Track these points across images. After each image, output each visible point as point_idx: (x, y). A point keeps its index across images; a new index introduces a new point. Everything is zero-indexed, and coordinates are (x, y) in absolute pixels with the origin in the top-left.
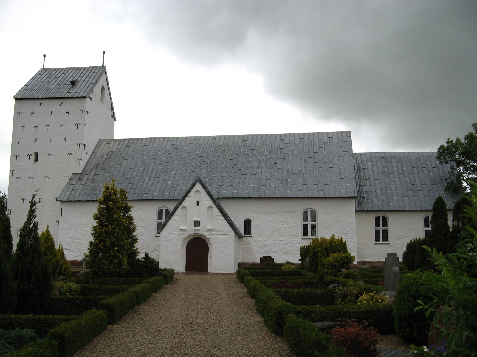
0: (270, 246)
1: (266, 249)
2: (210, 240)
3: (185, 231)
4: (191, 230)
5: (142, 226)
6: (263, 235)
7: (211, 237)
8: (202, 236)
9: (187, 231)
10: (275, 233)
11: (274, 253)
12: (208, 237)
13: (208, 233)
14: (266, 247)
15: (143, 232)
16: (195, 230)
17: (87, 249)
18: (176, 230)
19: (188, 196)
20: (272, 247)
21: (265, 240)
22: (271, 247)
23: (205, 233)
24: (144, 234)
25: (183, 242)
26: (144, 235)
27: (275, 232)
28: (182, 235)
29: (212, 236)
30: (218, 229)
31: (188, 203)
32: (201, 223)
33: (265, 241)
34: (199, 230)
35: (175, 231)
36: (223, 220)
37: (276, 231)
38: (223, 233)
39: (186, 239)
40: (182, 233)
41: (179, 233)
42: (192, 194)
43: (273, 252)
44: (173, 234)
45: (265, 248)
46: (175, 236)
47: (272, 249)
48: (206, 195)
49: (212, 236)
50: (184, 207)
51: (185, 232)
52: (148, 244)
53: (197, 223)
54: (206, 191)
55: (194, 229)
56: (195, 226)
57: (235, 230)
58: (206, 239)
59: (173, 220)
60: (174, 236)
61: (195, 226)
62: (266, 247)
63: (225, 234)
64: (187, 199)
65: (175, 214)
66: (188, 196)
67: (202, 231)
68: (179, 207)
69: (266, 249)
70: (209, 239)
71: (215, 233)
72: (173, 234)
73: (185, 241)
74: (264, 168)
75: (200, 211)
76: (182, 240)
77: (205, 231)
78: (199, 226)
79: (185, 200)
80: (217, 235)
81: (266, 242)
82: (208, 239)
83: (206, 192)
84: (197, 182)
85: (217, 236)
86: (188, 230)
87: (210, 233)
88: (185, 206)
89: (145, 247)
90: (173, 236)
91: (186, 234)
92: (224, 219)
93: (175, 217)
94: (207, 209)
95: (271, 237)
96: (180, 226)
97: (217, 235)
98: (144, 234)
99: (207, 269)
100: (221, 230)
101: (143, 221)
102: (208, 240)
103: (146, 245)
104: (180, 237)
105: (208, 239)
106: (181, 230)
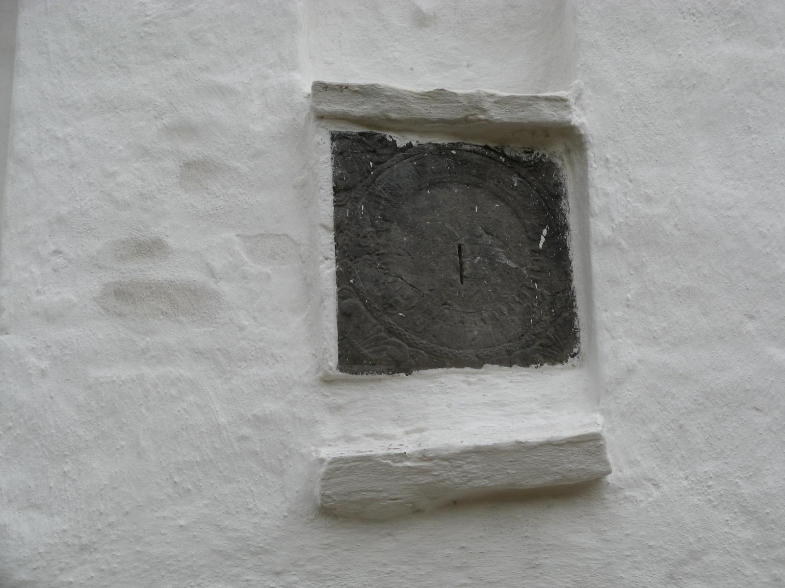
32: (614, 203)
56: (380, 337)
61: (380, 337)
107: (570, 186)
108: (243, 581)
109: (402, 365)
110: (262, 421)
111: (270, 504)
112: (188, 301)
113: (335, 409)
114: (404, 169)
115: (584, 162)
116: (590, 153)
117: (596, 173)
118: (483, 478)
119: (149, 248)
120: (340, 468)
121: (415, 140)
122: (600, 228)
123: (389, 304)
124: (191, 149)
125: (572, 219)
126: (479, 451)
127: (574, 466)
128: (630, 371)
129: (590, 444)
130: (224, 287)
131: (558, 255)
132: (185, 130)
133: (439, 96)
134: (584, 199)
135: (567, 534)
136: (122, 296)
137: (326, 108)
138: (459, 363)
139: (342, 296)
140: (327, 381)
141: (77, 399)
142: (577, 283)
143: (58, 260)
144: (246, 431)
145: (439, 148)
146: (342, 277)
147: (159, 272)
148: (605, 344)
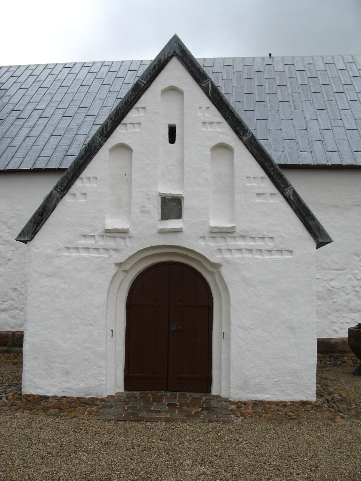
0: (342, 294)
1: (335, 302)
2: (224, 271)
3: (122, 235)
4: (148, 231)
5: (5, 241)
6: (325, 266)
7: (228, 262)
8: (190, 255)
9: (130, 237)
10: (355, 260)
11: (354, 313)
12: (215, 258)
13: (212, 244)
14: (334, 296)
15: (9, 255)
16: (162, 232)
17: (14, 299)
18: (88, 231)
19: (138, 105)
20: (351, 296)
21: (332, 277)
22: (347, 297)
23: (202, 243)
24: (9, 260)
25: (114, 276)
26: (11, 263)
27: (355, 257)
28: (112, 253)
29: (228, 256)
30: (255, 230)
31: (138, 130)
32: (186, 204)
33: (331, 280)
34: (178, 231)
35: (85, 236)
36: (272, 194)
37: (357, 255)
38: (270, 245)
39: (127, 267)
40: (111, 243)
41: (101, 243)
42: (151, 97)
43: (352, 310)
44: (77, 248)
45: (332, 299)
46: (84, 254)
47: (348, 301)
48: (206, 102)
49: (228, 256)
50: (123, 147)
51: (124, 238)
52: (19, 288)
53: (171, 207)
54: (206, 90)
55: (160, 227)
56: (164, 216)
57: (317, 234)
58: (206, 269)
59: (78, 194)
60: (82, 257)
61: (164, 216)
62: (334, 296)
63: (282, 246)
64: (132, 116)
65: (87, 173)
66: (138, 105)
67: (191, 234)
68: (101, 145)
69: (335, 300)
70: (217, 266)
71: (240, 243)
72: (77, 248)
73: (121, 276)
74: (307, 109)
75: (182, 162)
76: (113, 270)
77: (203, 238)
78: (179, 215)
79: (126, 120)
80: (250, 250)
81: (333, 283)
82: (209, 268)
83: (207, 94)
84: (171, 57)
85: (248, 255)
86: (133, 232)
87: (222, 244)
88: (127, 142)
89: (13, 294)
90: (75, 254)
91: (129, 248)
92: (274, 190)
93: (87, 185)
94: (209, 153)
95: (345, 271)
96: (104, 218)
97: (250, 250)
98: (9, 260)
99: (204, 382)
100: (265, 233)
101: (9, 228)
102: (212, 273)
103: (16, 289)
104: (105, 259)
105: (209, 268)
106: (107, 231)
107: (182, 202)
108: (224, 415)
109: (166, 219)
110: (154, 224)
111: (155, 231)
112: (147, 212)
113: (160, 223)
114: (167, 200)
115: (184, 199)
116: (184, 199)
117: (185, 201)
118: (172, 230)
119: (144, 207)
120: (161, 229)
121: (168, 197)
122: (184, 207)
123: (165, 214)
124: (148, 196)
125: (182, 205)
126: (172, 229)
127: (180, 230)
128: (186, 221)
129: (181, 228)
130: (151, 211)
131: (181, 209)
132: (147, 194)
133: (170, 194)
134: (183, 204)
135: (179, 235)
136: (142, 211)
137: (160, 195)
138: (171, 219)
139: (161, 213)
140: (160, 220)
141: (49, 81)
142: (182, 211)
143: (136, 208)
144: (153, 225)
145: (170, 198)
146: (161, 211)
147: (145, 209)
148: (184, 218)
